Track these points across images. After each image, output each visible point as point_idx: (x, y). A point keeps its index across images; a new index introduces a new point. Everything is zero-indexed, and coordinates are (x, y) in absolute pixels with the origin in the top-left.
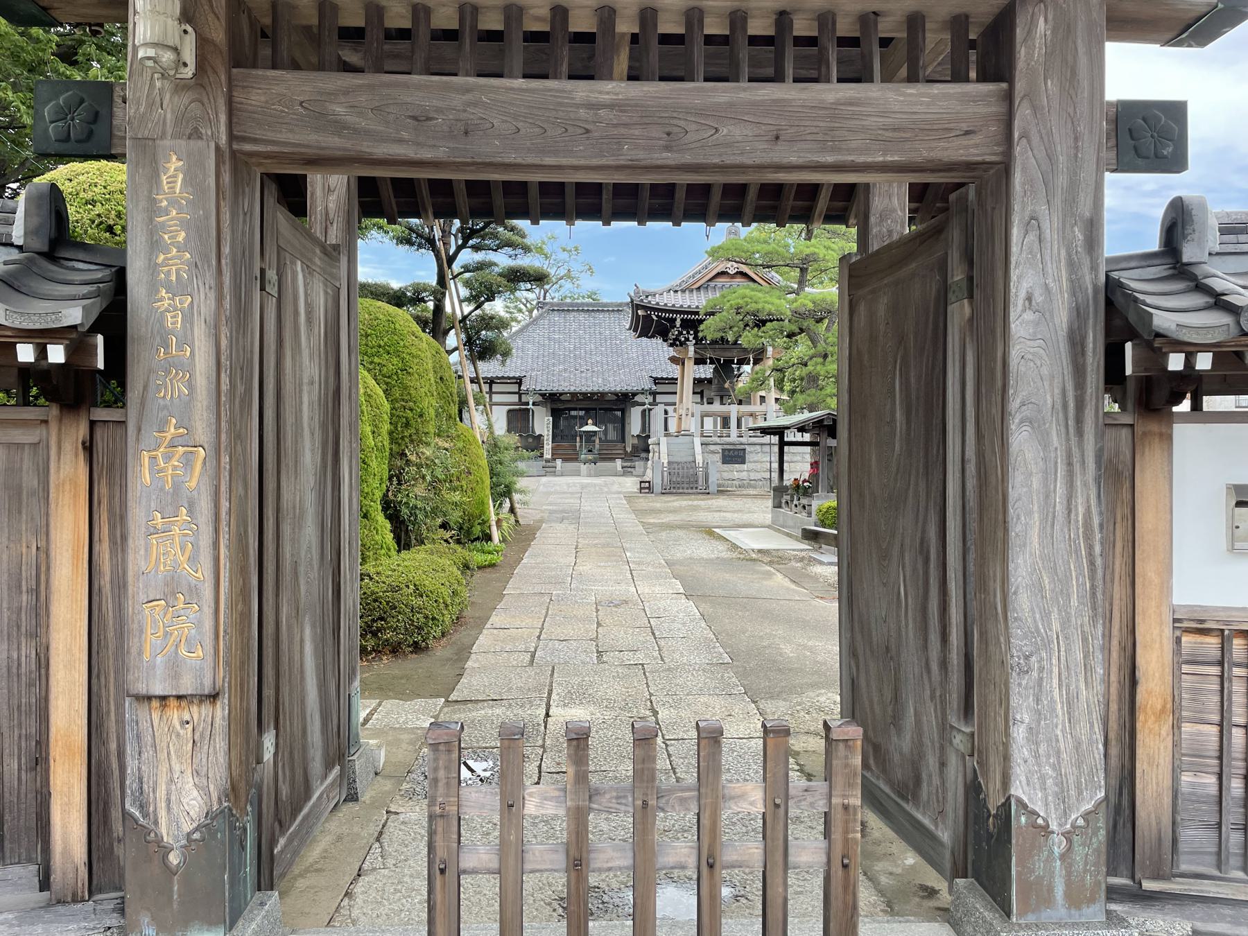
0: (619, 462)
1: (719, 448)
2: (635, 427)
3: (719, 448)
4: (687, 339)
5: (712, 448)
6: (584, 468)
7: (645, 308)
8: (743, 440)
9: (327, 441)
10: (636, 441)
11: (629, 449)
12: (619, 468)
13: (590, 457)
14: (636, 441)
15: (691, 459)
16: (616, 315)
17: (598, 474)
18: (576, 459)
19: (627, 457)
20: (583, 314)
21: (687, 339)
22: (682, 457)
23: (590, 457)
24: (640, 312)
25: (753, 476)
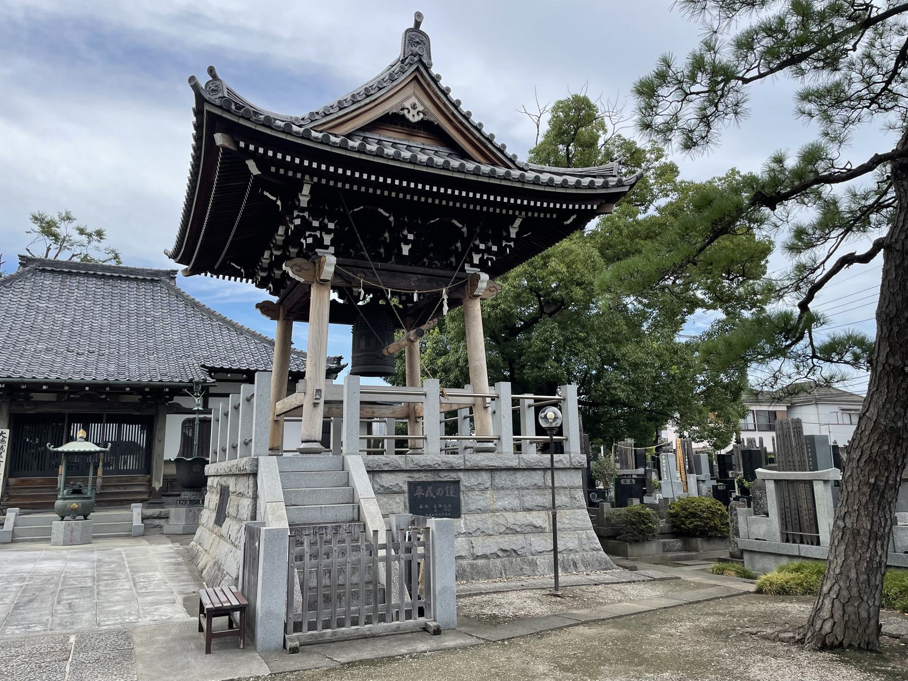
0: (136, 511)
1: (401, 481)
2: (171, 446)
3: (401, 481)
4: (319, 243)
5: (388, 480)
6: (59, 527)
7: (232, 129)
8: (455, 460)
9: (106, 501)
10: (172, 470)
11: (157, 485)
12: (137, 521)
13: (74, 504)
14: (172, 470)
15: (346, 512)
16: (149, 286)
17: (87, 539)
18: (48, 506)
19: (152, 498)
20: (94, 281)
21: (319, 243)
22: (324, 510)
23: (74, 504)
24: (220, 139)
25: (484, 546)
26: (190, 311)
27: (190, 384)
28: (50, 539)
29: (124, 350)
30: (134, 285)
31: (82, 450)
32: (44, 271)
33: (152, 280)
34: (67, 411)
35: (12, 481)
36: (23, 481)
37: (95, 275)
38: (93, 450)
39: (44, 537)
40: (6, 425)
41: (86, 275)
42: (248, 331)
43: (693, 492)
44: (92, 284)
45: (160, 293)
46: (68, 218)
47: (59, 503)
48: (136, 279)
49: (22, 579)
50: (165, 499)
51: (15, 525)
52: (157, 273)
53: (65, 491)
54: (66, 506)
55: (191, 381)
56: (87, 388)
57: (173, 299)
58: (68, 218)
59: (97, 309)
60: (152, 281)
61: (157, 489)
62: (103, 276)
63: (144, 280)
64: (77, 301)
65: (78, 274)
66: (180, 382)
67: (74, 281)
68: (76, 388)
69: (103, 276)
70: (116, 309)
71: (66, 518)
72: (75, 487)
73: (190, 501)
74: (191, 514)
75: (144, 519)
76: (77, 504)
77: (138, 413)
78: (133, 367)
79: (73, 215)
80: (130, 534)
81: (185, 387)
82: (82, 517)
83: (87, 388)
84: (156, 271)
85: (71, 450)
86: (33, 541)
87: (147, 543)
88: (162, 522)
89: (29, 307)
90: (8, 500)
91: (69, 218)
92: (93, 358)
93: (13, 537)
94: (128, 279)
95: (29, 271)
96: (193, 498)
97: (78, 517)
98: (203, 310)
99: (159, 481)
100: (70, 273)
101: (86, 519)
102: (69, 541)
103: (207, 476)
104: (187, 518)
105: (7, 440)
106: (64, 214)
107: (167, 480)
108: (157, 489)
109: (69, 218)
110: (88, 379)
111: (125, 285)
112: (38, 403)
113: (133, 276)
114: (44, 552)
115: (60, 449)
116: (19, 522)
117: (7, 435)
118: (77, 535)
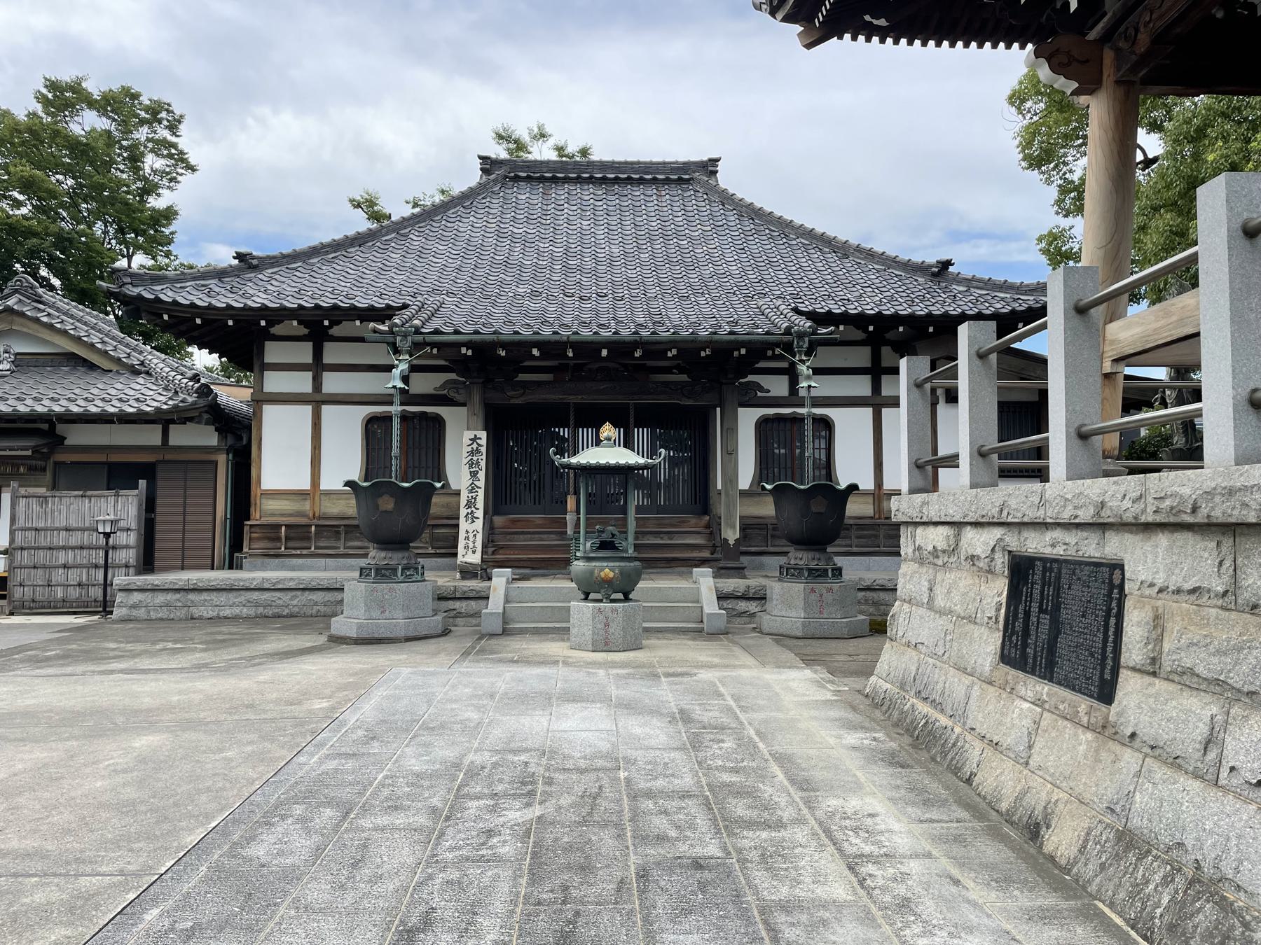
6: (583, 613)
11: (731, 535)
13: (607, 570)
16: (676, 190)
18: (556, 564)
19: (724, 560)
23: (607, 570)
26: (748, 225)
27: (786, 338)
28: (567, 630)
29: (652, 291)
30: (652, 191)
31: (613, 462)
32: (516, 179)
33: (680, 179)
34: (572, 399)
35: (499, 520)
36: (514, 521)
37: (591, 180)
38: (632, 462)
39: (555, 627)
40: (480, 424)
41: (579, 180)
42: (858, 249)
43: (271, 505)
44: (588, 194)
45: (694, 199)
46: (543, 135)
47: (578, 566)
48: (655, 181)
49: (526, 788)
50: (745, 560)
51: (507, 601)
52: (686, 167)
53: (588, 544)
54: (592, 573)
55: (788, 331)
56: (604, 353)
57: (717, 208)
58: (543, 135)
59: (600, 232)
60: (680, 181)
61: (731, 542)
62: (604, 180)
63: (667, 181)
64: (569, 222)
65: (566, 180)
66: (768, 333)
67: (561, 192)
68: (588, 349)
69: (604, 180)
70: (629, 230)
71: (592, 596)
72: (605, 537)
73: (810, 570)
74: (813, 597)
75: (722, 597)
76: (612, 569)
77: (690, 402)
78: (675, 316)
79: (548, 129)
80: (699, 631)
81: (777, 345)
82: (620, 596)
83: (604, 353)
84: (684, 163)
85: (593, 462)
86: (537, 632)
87: (750, 660)
88: (752, 607)
89: (499, 235)
90: (493, 553)
91: (543, 136)
92: (605, 305)
93: (505, 622)
94: (641, 181)
95: (495, 181)
96: (813, 565)
97: (614, 596)
98: (771, 222)
99: (734, 527)
100: (554, 180)
101: (627, 598)
102: (603, 644)
103: (898, 526)
104: (807, 604)
105: (484, 450)
106: (536, 130)
107: (749, 527)
108: (731, 542)
109: (543, 136)
110: (606, 334)
111: (638, 192)
112: (525, 385)
113: (649, 177)
114: (562, 671)
115: (574, 460)
116: (513, 594)
117: (484, 442)
118: (616, 629)
